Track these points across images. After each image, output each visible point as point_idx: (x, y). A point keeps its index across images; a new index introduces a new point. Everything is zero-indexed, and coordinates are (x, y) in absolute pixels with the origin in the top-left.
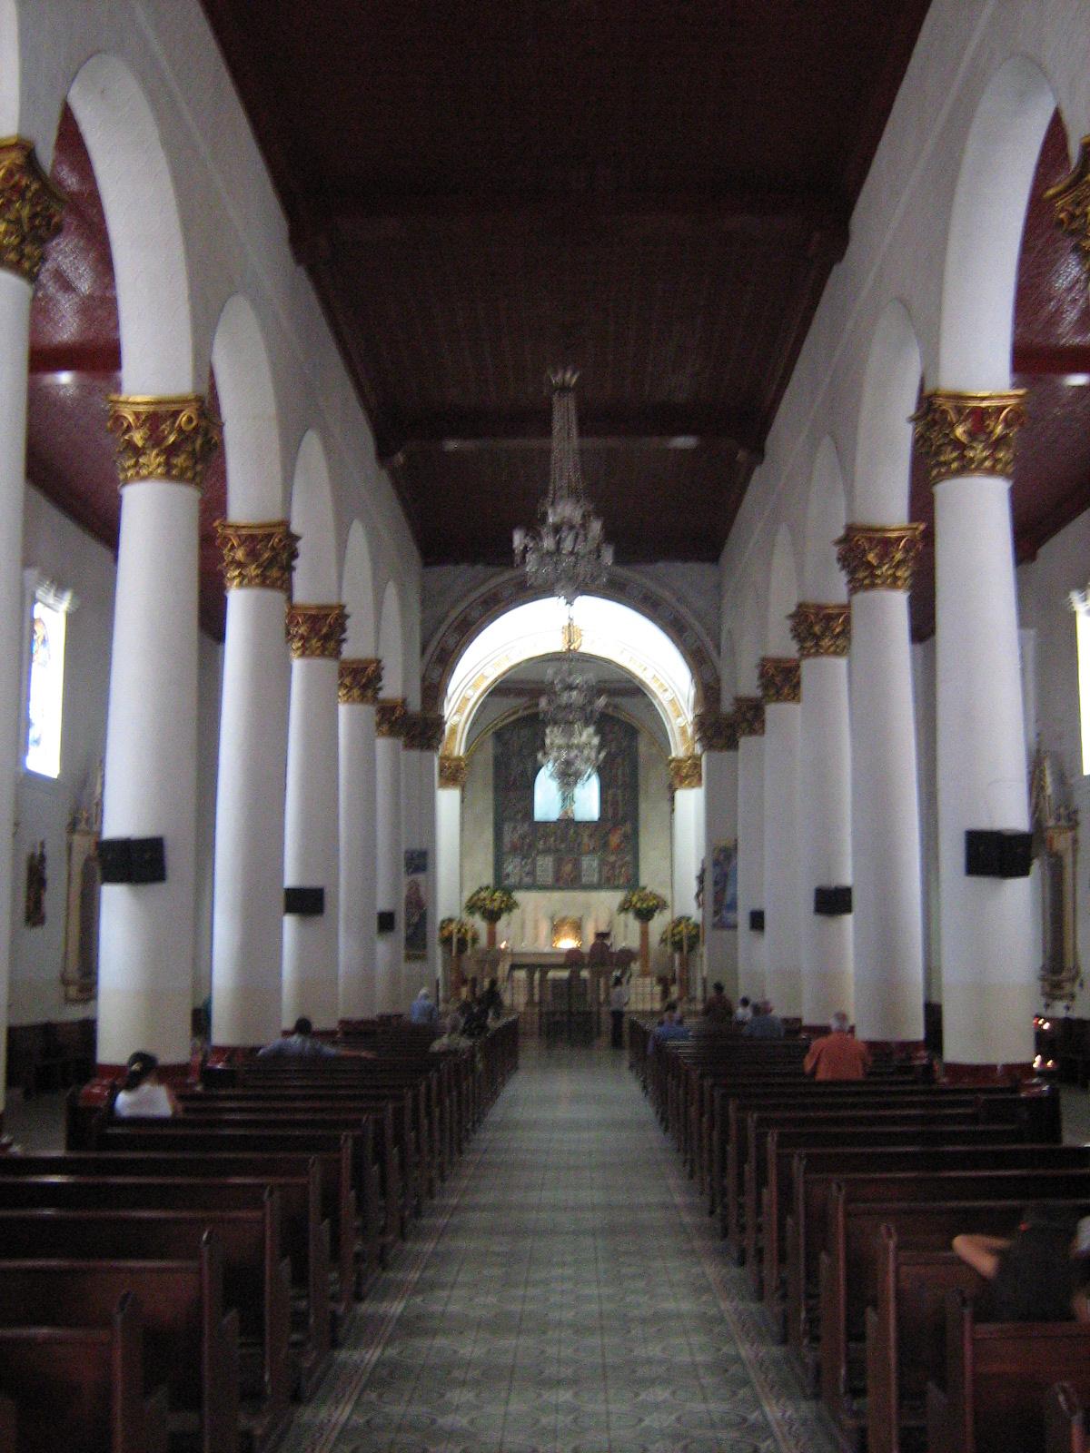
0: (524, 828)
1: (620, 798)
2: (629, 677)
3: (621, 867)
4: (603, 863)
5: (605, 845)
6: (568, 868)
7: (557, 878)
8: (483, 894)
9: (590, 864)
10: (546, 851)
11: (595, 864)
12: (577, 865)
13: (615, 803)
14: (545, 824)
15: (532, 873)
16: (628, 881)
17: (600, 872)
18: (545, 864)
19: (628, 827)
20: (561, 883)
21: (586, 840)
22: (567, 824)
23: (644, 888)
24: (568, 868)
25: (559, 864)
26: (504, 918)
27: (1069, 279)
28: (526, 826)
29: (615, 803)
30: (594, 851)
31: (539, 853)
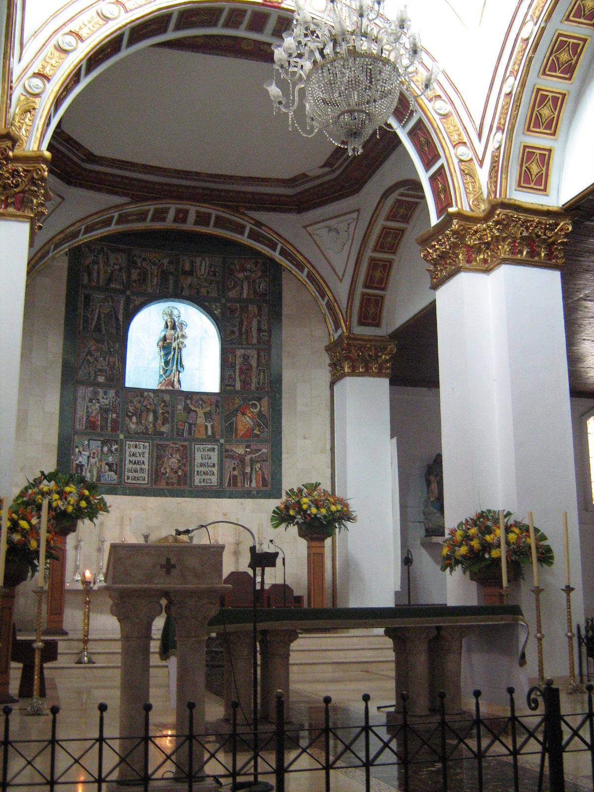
0: (108, 398)
1: (254, 363)
2: (86, 59)
3: (253, 462)
4: (225, 455)
5: (230, 429)
6: (174, 461)
7: (156, 475)
8: (45, 486)
9: (206, 459)
10: (142, 436)
11: (215, 457)
12: (187, 457)
13: (246, 370)
14: (139, 392)
15: (117, 468)
16: (265, 484)
17: (221, 469)
18: (138, 454)
19: (264, 406)
20: (163, 485)
21: (201, 420)
22: (171, 400)
23: (294, 525)
24: (174, 461)
25: (158, 458)
26: (84, 525)
27: (150, 275)
28: (112, 393)
29: (246, 370)
30: (212, 439)
31: (130, 436)
